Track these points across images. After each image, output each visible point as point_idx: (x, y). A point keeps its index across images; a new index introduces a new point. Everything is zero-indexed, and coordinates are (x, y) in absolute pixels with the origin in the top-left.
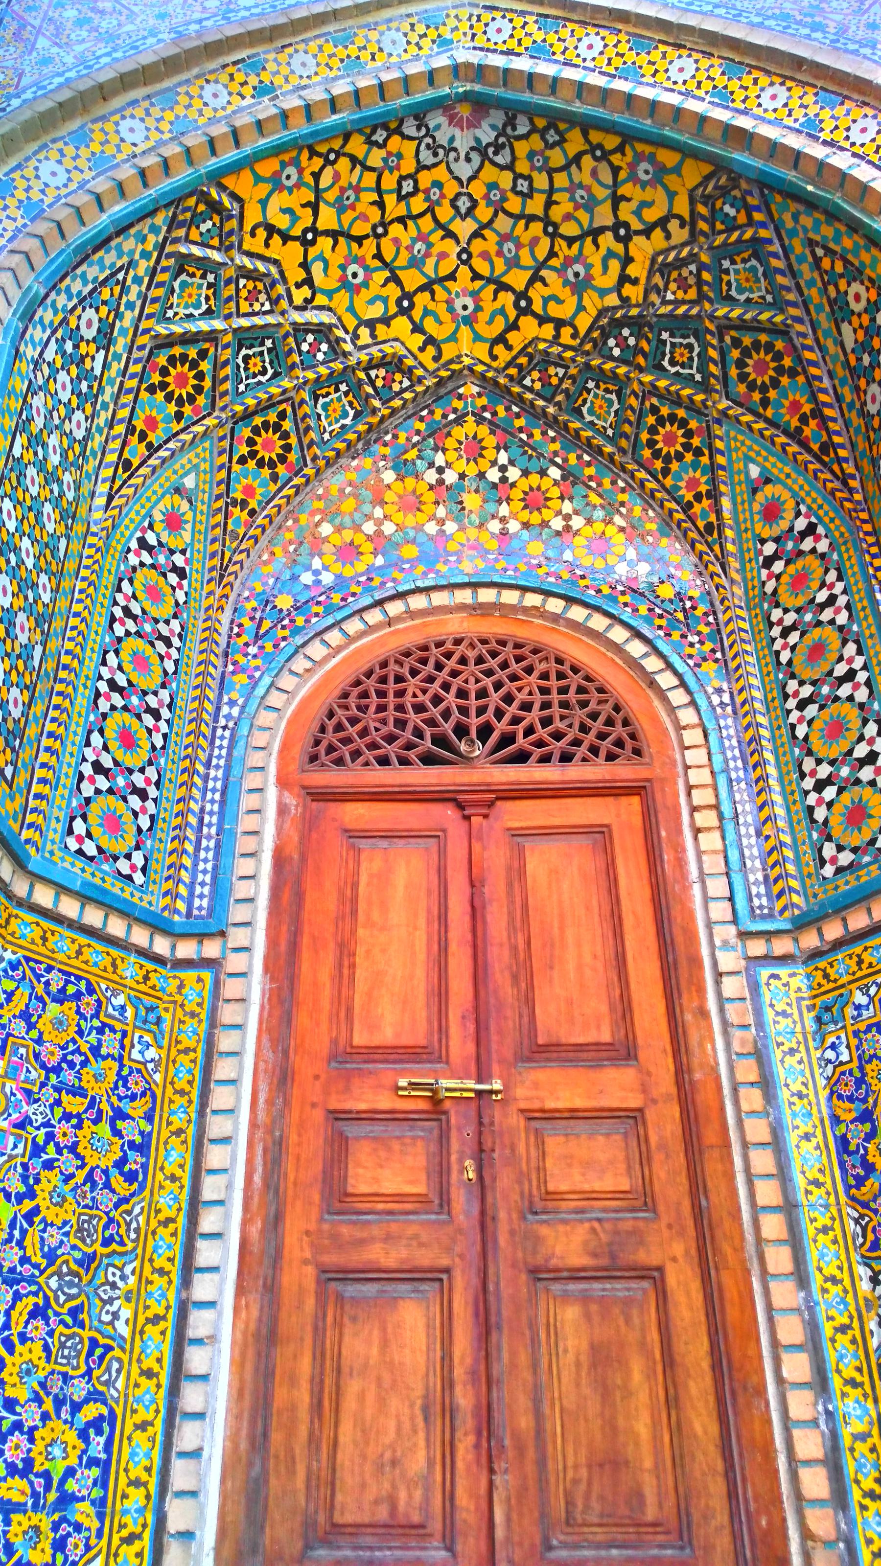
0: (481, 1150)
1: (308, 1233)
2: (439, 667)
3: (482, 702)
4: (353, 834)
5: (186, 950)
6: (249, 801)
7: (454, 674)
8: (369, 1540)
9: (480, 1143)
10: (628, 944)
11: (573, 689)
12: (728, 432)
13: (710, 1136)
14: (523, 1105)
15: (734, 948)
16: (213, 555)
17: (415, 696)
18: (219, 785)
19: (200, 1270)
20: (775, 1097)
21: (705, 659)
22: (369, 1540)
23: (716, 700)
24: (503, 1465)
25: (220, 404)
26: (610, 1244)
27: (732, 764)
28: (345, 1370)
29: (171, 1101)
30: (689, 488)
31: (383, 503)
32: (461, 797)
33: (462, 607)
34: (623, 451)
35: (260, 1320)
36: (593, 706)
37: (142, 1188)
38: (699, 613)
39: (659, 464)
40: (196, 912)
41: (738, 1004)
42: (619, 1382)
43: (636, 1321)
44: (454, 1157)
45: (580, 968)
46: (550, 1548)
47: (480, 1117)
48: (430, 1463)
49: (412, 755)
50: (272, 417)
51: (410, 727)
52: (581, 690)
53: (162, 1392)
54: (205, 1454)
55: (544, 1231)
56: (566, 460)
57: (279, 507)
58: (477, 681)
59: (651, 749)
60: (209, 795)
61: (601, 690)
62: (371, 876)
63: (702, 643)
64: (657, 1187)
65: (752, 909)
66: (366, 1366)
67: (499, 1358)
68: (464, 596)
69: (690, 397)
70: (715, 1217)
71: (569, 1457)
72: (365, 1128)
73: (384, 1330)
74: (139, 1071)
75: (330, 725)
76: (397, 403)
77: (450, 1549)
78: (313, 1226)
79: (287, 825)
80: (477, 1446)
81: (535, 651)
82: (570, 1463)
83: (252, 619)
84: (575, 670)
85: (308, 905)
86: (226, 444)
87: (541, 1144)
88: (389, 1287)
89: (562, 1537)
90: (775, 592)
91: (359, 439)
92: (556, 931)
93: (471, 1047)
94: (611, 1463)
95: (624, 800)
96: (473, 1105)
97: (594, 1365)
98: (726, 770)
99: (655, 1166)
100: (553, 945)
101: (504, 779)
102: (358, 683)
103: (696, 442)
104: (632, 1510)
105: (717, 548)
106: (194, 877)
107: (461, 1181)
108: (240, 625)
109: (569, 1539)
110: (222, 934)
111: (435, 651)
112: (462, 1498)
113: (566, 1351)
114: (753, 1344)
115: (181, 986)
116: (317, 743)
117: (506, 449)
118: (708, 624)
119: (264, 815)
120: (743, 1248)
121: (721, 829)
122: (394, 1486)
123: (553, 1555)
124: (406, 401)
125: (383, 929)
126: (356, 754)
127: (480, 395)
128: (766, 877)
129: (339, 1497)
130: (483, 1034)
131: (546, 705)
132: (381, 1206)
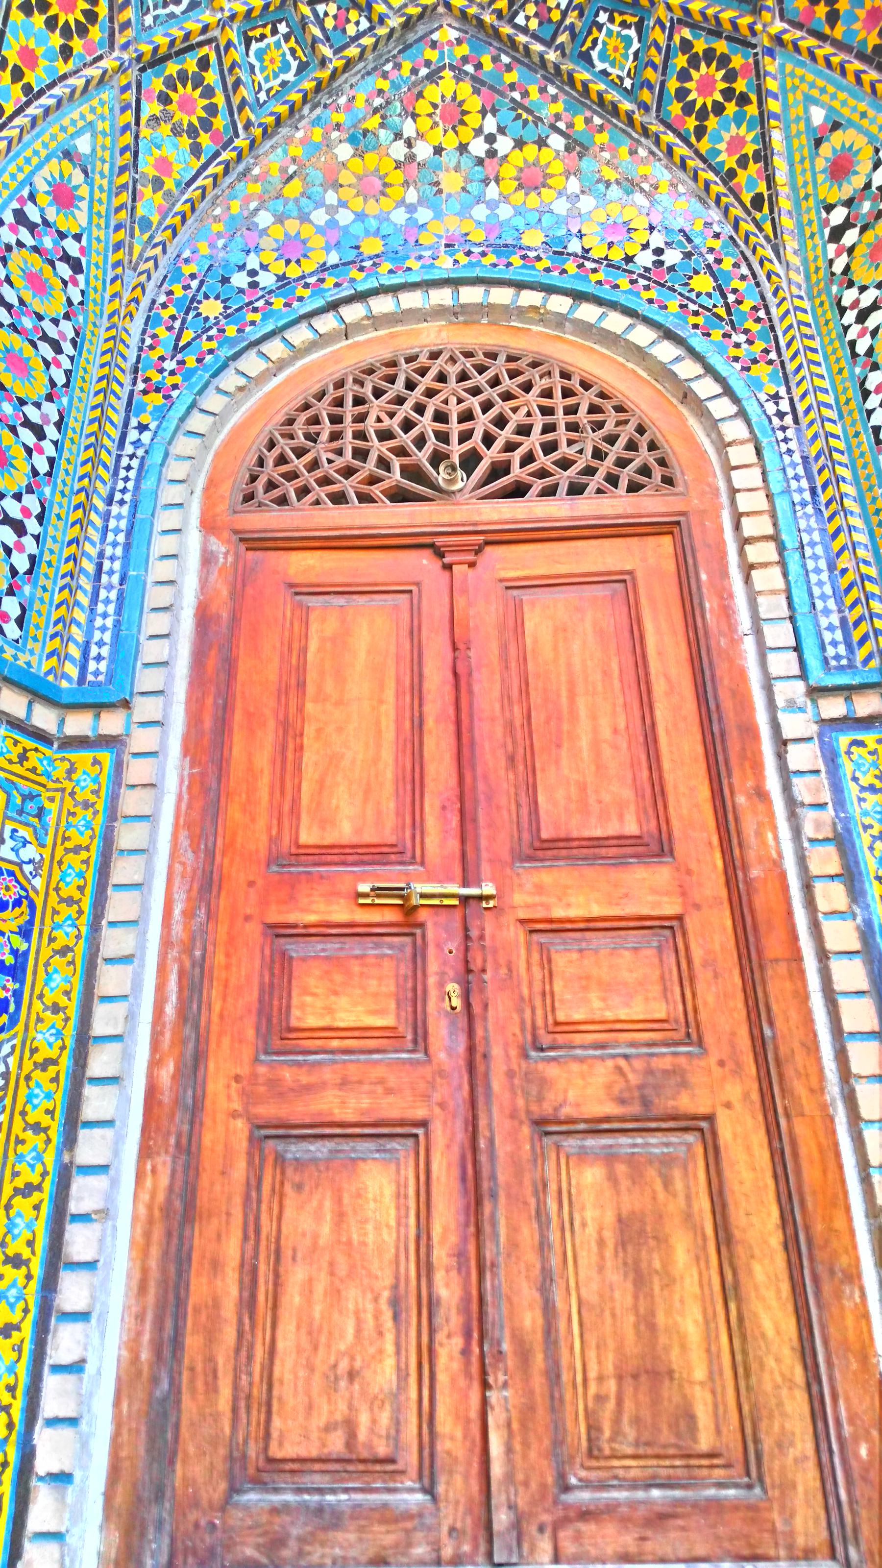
0: (469, 971)
1: (237, 1078)
2: (410, 386)
3: (466, 426)
4: (298, 590)
5: (79, 724)
6: (162, 545)
7: (430, 393)
8: (318, 1480)
9: (467, 962)
10: (658, 714)
11: (584, 409)
12: (782, 66)
13: (773, 946)
14: (522, 914)
15: (802, 710)
16: (118, 246)
17: (379, 420)
18: (123, 524)
19: (89, 1124)
20: (863, 893)
21: (755, 361)
22: (318, 1480)
23: (771, 408)
24: (501, 1378)
25: (121, 40)
26: (641, 1087)
27: (794, 484)
28: (287, 1253)
29: (55, 912)
30: (730, 151)
31: (337, 186)
32: (439, 541)
33: (440, 312)
34: (644, 107)
35: (170, 1189)
36: (609, 427)
37: (14, 1020)
38: (746, 307)
39: (691, 123)
40: (90, 678)
41: (810, 779)
42: (657, 1265)
43: (679, 1185)
44: (432, 980)
45: (596, 745)
46: (567, 1488)
47: (466, 929)
48: (402, 1374)
49: (376, 490)
50: (191, 65)
51: (373, 457)
52: (593, 409)
53: (34, 1285)
54: (90, 1368)
55: (552, 1071)
56: (570, 125)
57: (204, 189)
58: (460, 401)
59: (684, 476)
60: (110, 537)
61: (619, 409)
62: (323, 640)
63: (750, 342)
64: (703, 1016)
65: (826, 661)
66: (315, 1247)
67: (495, 1235)
68: (443, 297)
69: (733, 23)
70: (783, 1050)
71: (593, 1363)
72: (318, 947)
73: (339, 1201)
74: (11, 873)
75: (271, 458)
76: (353, 51)
77: (430, 1491)
78: (244, 1070)
79: (213, 577)
80: (466, 1352)
81: (535, 365)
82: (592, 1374)
83: (170, 329)
84: (586, 385)
85: (241, 676)
86: (130, 96)
87: (547, 962)
88: (346, 1146)
89: (583, 1474)
90: (847, 269)
91: (305, 101)
92: (564, 700)
93: (454, 844)
94: (649, 1372)
95: (651, 541)
96: (457, 915)
97: (622, 1244)
98: (787, 491)
99: (700, 987)
100: (560, 719)
101: (495, 517)
102: (306, 407)
103: (740, 85)
104: (678, 1435)
105: (768, 227)
106: (89, 633)
107: (440, 1010)
108: (154, 336)
109: (593, 1475)
110: (126, 704)
111: (404, 366)
112: (445, 1423)
113: (584, 1225)
114: (840, 1214)
115: (71, 771)
116: (253, 479)
117: (494, 112)
118: (758, 320)
119: (180, 564)
120: (822, 1090)
121: (782, 563)
122: (350, 1407)
123: (571, 1498)
124: (364, 49)
125: (339, 703)
126: (303, 491)
127: (459, 42)
128: (843, 621)
129: (277, 1423)
130: (469, 827)
131: (548, 428)
132: (335, 1043)
